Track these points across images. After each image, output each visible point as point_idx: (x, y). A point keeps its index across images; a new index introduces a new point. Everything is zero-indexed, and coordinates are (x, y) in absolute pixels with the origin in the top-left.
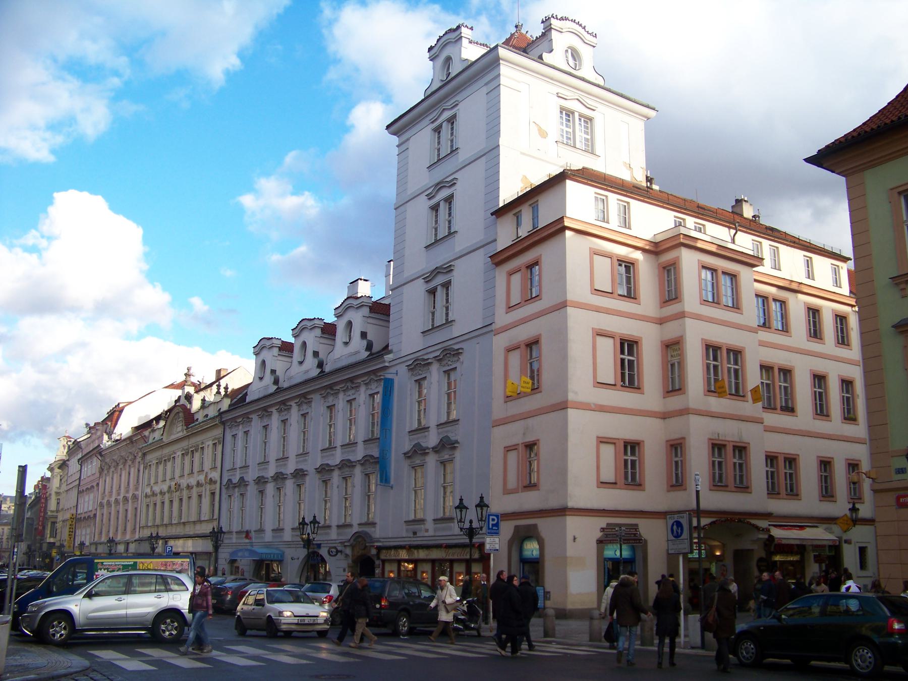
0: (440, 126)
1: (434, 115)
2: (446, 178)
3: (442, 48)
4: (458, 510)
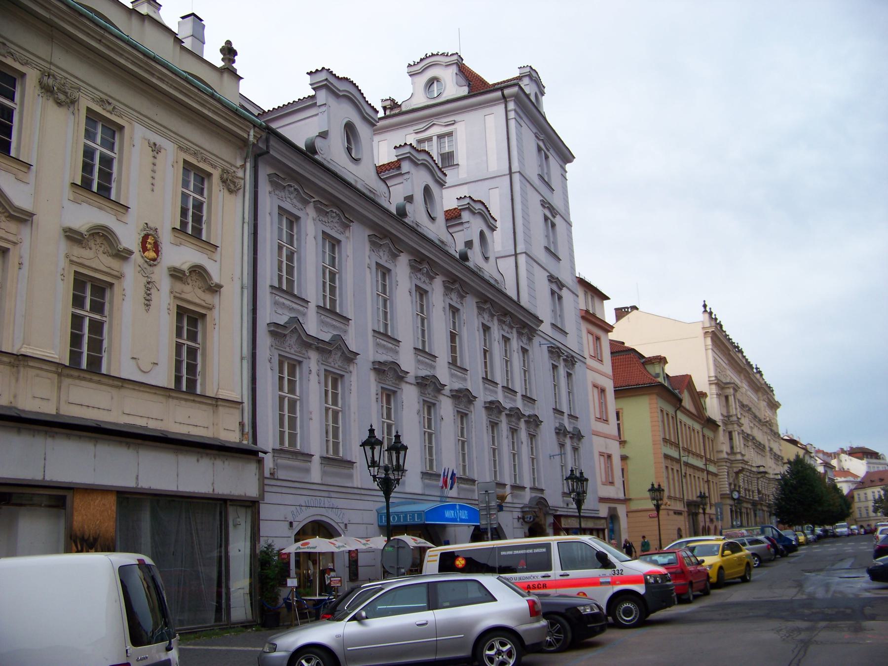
4: (368, 448)
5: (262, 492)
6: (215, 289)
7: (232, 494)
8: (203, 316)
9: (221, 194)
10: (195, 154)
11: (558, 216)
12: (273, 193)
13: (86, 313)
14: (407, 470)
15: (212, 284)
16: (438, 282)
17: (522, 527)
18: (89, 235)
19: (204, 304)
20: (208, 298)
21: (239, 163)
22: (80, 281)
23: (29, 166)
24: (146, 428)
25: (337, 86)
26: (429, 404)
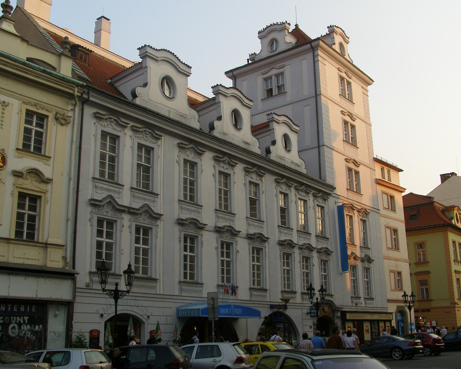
0: (270, 78)
1: (266, 70)
2: (355, 115)
3: (268, 33)
4: (404, 297)
5: (74, 296)
6: (48, 181)
7: (51, 297)
8: (40, 197)
9: (54, 128)
10: (35, 105)
11: (358, 120)
12: (97, 123)
13: (27, 212)
14: (316, 294)
15: (44, 178)
16: (240, 167)
17: (311, 318)
18: (26, 173)
19: (39, 190)
20: (43, 186)
21: (70, 107)
22: (22, 196)
23: (50, 157)
24: (23, 264)
25: (223, 91)
26: (353, 266)
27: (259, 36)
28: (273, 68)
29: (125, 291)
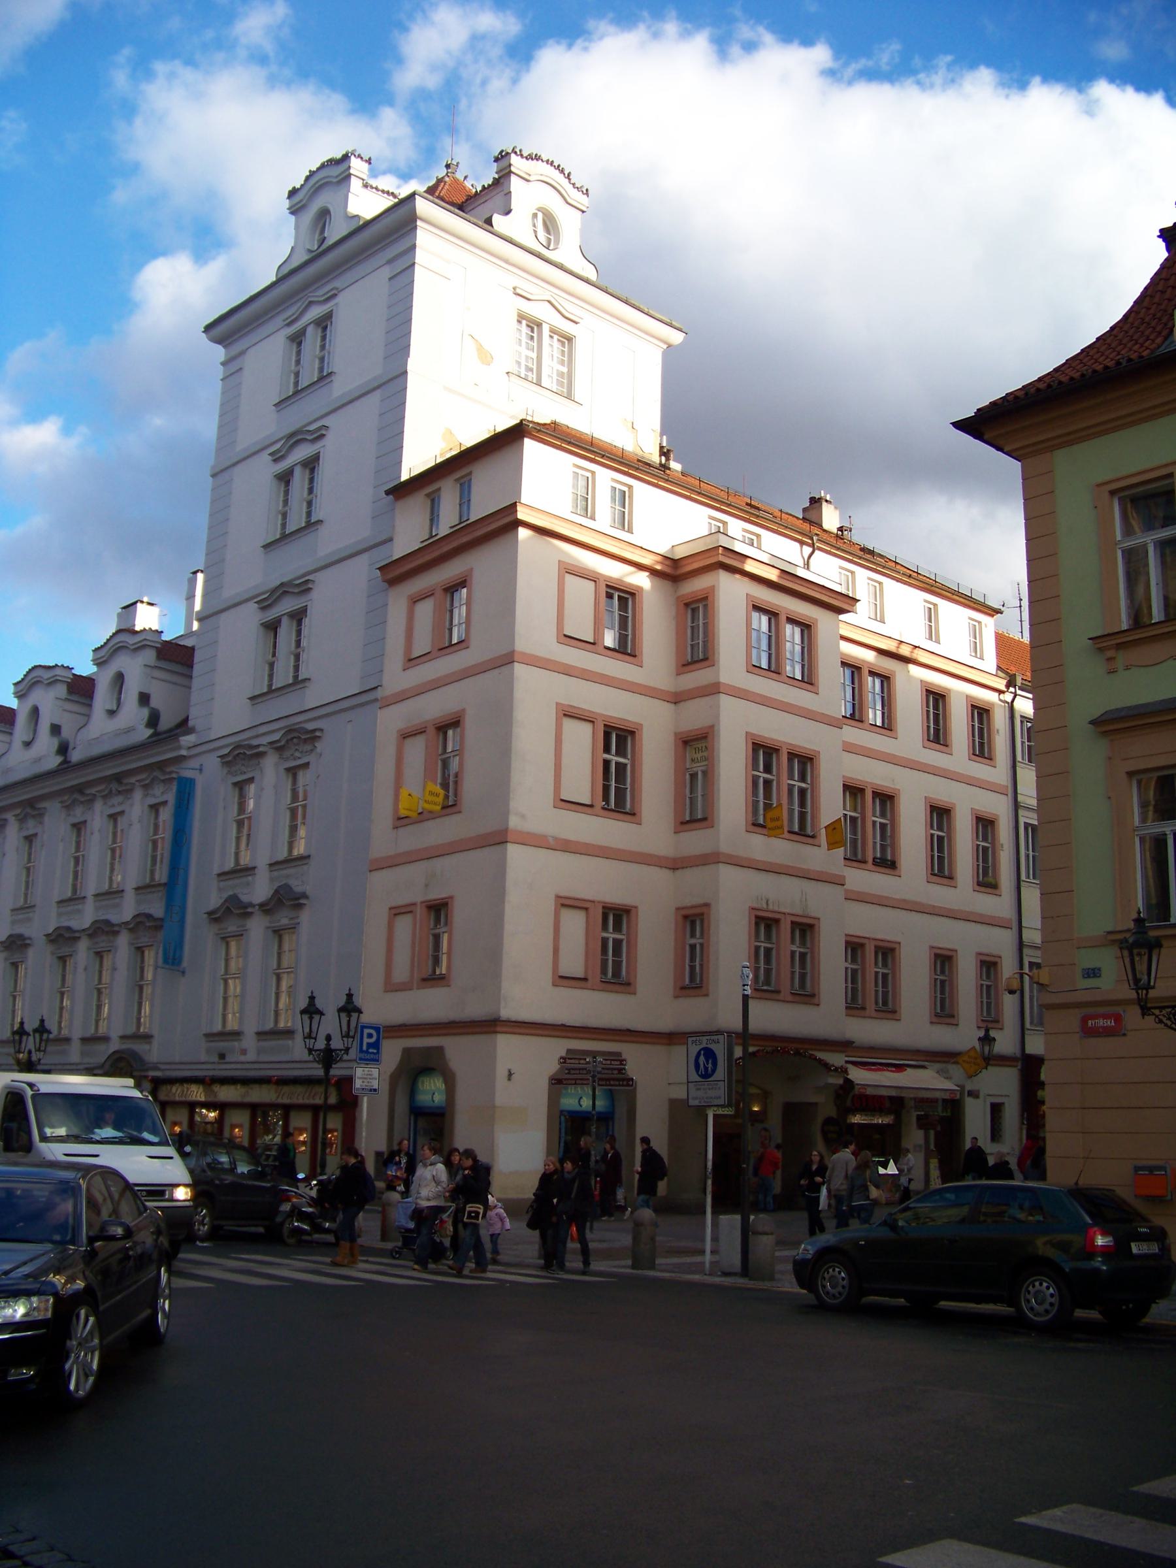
0: (302, 333)
4: (306, 1017)
27: (500, 168)
28: (311, 303)
29: (341, 1050)
